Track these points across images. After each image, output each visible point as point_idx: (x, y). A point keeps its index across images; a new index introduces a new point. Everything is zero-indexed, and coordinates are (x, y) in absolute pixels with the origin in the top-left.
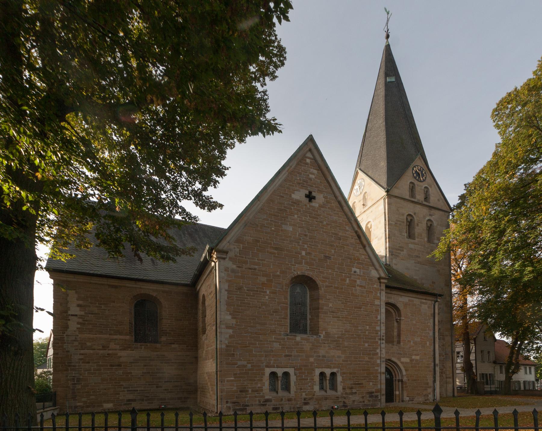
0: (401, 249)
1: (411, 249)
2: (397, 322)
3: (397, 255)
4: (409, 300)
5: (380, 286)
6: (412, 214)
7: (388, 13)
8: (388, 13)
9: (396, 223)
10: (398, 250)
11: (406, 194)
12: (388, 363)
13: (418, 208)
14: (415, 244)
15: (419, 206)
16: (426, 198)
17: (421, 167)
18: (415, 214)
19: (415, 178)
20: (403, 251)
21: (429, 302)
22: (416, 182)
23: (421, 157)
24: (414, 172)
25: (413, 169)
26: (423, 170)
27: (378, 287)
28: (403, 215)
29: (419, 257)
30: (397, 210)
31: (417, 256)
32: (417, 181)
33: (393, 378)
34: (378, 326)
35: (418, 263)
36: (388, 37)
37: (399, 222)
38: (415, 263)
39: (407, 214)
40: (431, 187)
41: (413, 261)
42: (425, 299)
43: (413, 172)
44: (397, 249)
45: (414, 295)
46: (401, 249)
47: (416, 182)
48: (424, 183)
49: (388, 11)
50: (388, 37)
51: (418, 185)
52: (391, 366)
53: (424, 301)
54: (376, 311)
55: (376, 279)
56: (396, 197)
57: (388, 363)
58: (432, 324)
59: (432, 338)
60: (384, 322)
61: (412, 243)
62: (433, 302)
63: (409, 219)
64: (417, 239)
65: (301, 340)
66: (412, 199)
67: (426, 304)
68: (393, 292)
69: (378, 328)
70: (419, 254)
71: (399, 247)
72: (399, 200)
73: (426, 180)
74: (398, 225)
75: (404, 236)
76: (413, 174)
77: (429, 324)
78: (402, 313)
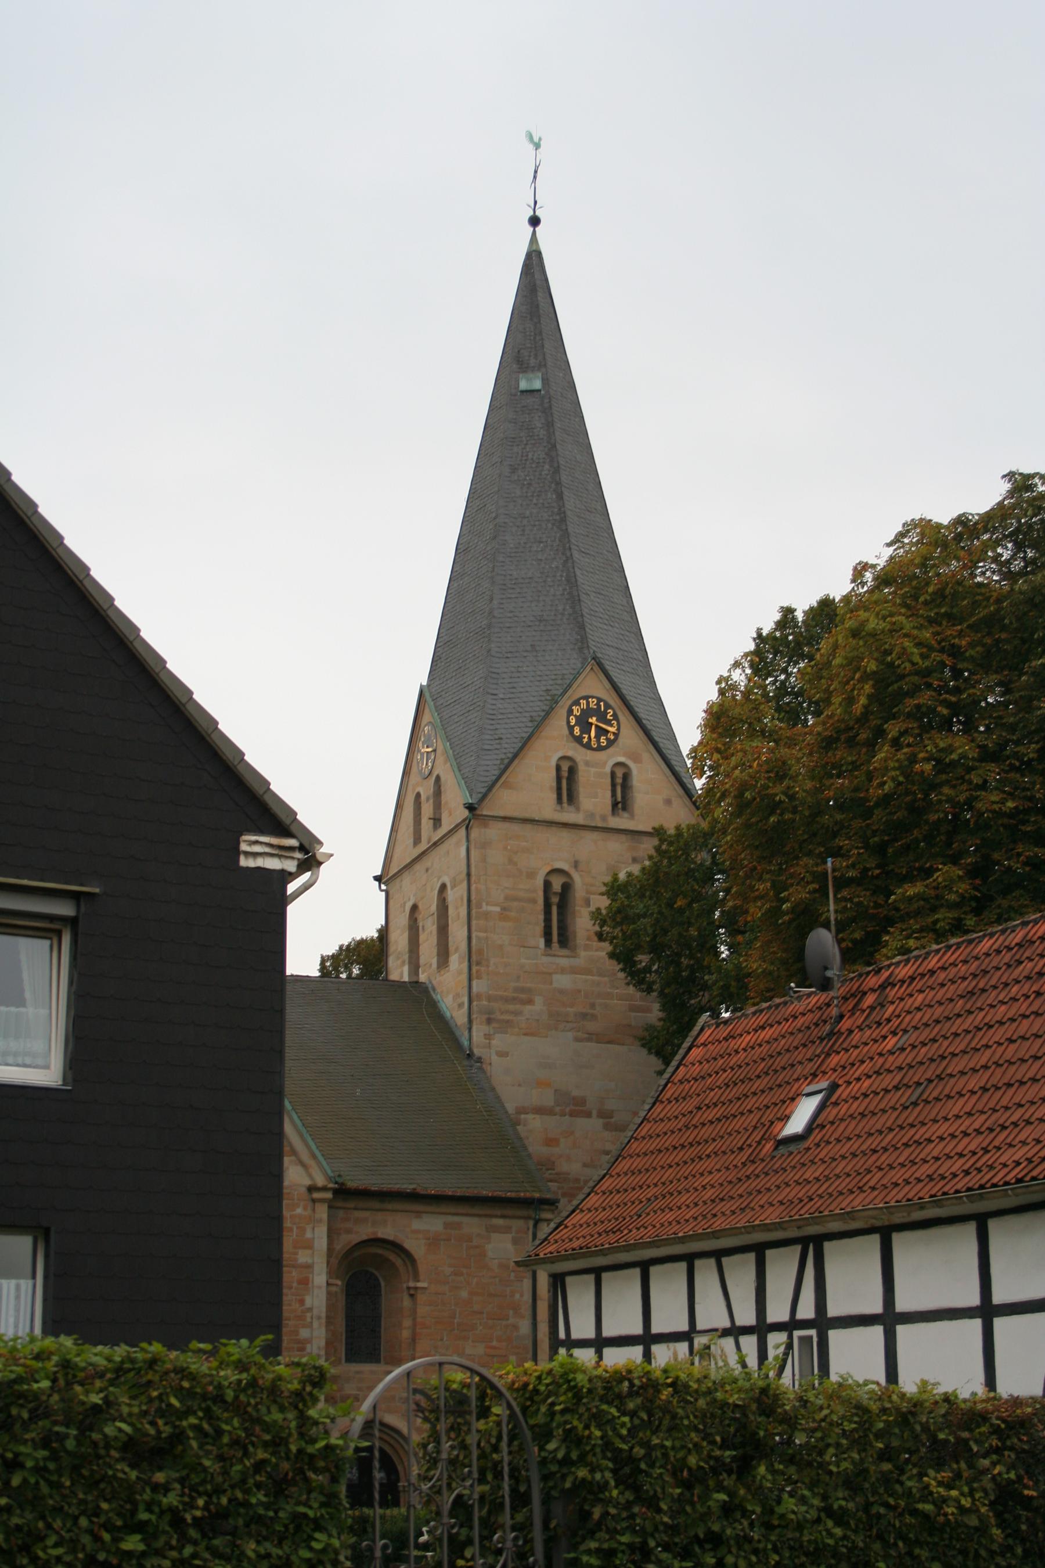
0: (523, 996)
1: (561, 991)
2: (412, 1296)
3: (508, 1021)
4: (446, 1225)
5: (314, 1210)
6: (565, 866)
7: (537, 146)
8: (537, 146)
9: (504, 909)
10: (514, 1000)
11: (546, 806)
12: (385, 1437)
13: (589, 845)
14: (574, 971)
15: (590, 836)
16: (621, 803)
17: (599, 700)
18: (576, 864)
19: (578, 740)
20: (530, 1002)
21: (520, 1223)
22: (580, 755)
23: (596, 668)
24: (573, 722)
25: (570, 712)
26: (608, 706)
27: (309, 1212)
28: (531, 875)
29: (594, 1017)
30: (511, 861)
31: (584, 1016)
32: (583, 750)
33: (398, 1480)
34: (304, 1326)
35: (589, 1040)
36: (535, 221)
37: (515, 904)
38: (577, 1040)
39: (549, 869)
40: (637, 759)
41: (570, 1035)
42: (503, 1217)
43: (568, 722)
44: (507, 1000)
45: (461, 1209)
46: (523, 996)
47: (580, 755)
48: (611, 750)
49: (536, 140)
50: (535, 221)
51: (587, 764)
52: (389, 1444)
53: (500, 1222)
54: (300, 1282)
55: (304, 1190)
56: (505, 819)
57: (385, 1437)
58: (527, 1297)
59: (529, 1343)
60: (324, 1315)
61: (563, 971)
62: (531, 1223)
63: (557, 885)
64: (583, 954)
65: (445, 1228)
66: (569, 816)
67: (507, 1230)
68: (390, 1206)
69: (304, 1333)
70: (593, 1006)
71: (517, 990)
72: (516, 828)
73: (620, 740)
74: (513, 914)
75: (537, 947)
76: (571, 729)
77: (517, 1296)
78: (422, 1268)
